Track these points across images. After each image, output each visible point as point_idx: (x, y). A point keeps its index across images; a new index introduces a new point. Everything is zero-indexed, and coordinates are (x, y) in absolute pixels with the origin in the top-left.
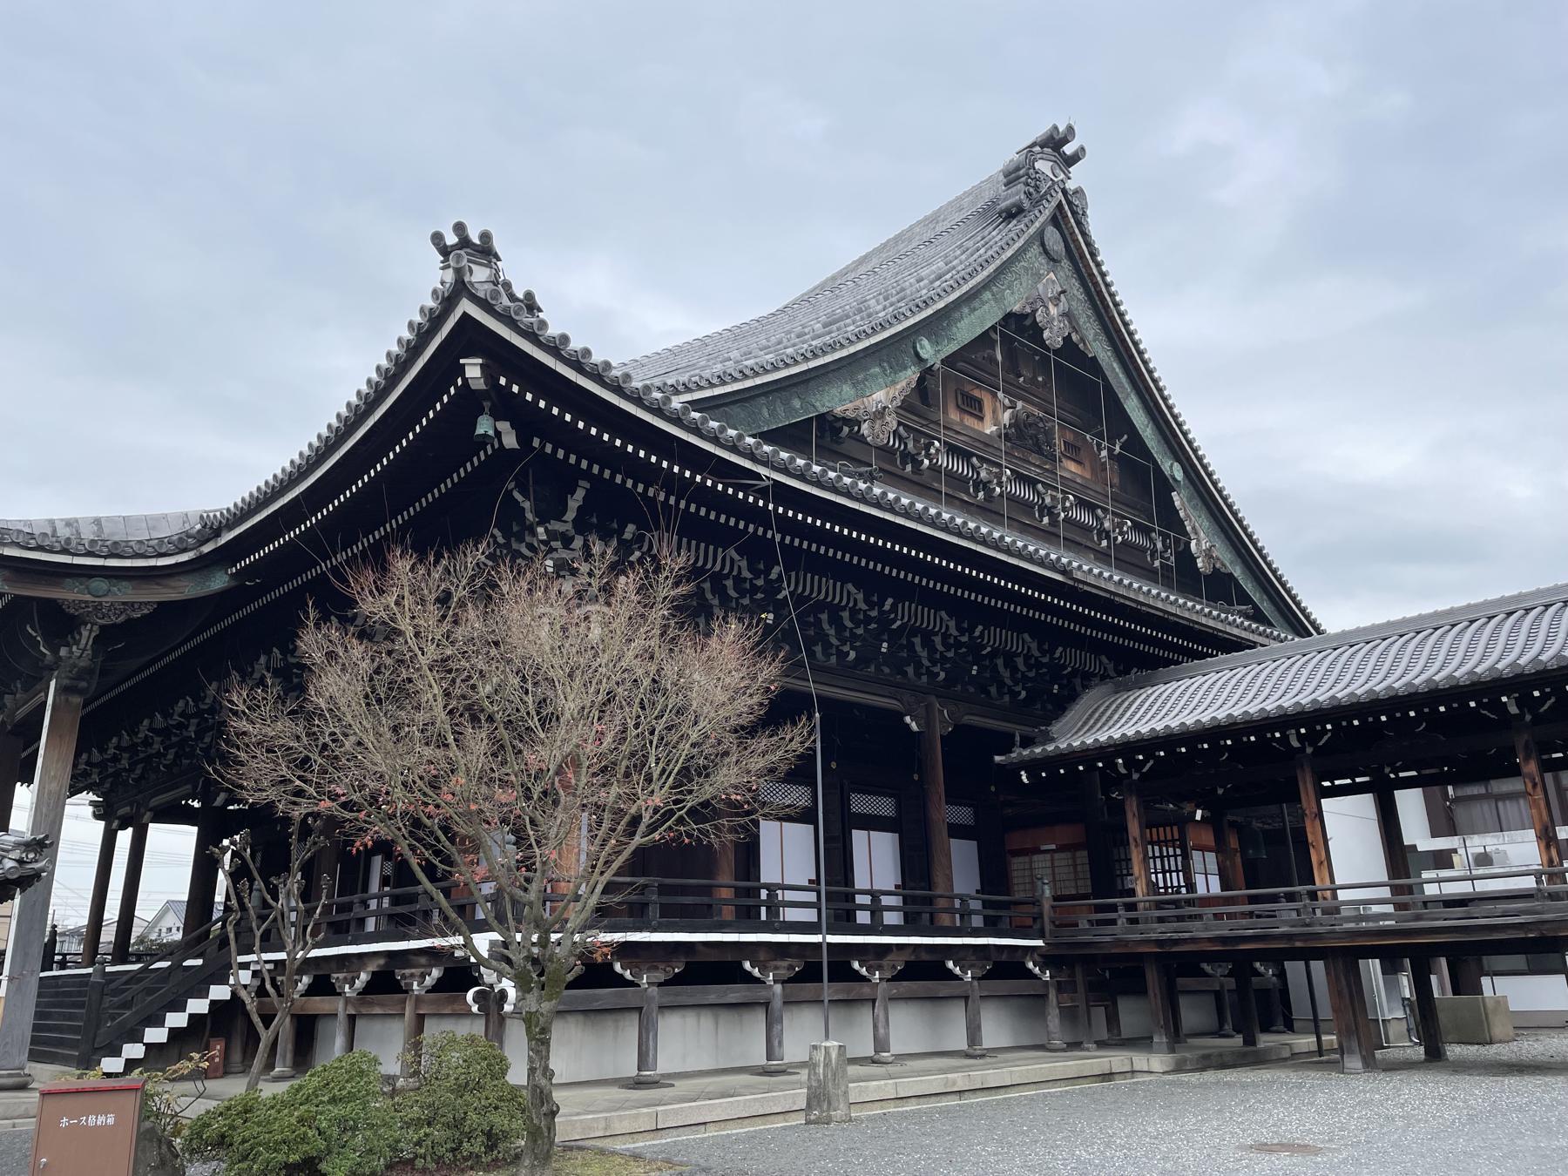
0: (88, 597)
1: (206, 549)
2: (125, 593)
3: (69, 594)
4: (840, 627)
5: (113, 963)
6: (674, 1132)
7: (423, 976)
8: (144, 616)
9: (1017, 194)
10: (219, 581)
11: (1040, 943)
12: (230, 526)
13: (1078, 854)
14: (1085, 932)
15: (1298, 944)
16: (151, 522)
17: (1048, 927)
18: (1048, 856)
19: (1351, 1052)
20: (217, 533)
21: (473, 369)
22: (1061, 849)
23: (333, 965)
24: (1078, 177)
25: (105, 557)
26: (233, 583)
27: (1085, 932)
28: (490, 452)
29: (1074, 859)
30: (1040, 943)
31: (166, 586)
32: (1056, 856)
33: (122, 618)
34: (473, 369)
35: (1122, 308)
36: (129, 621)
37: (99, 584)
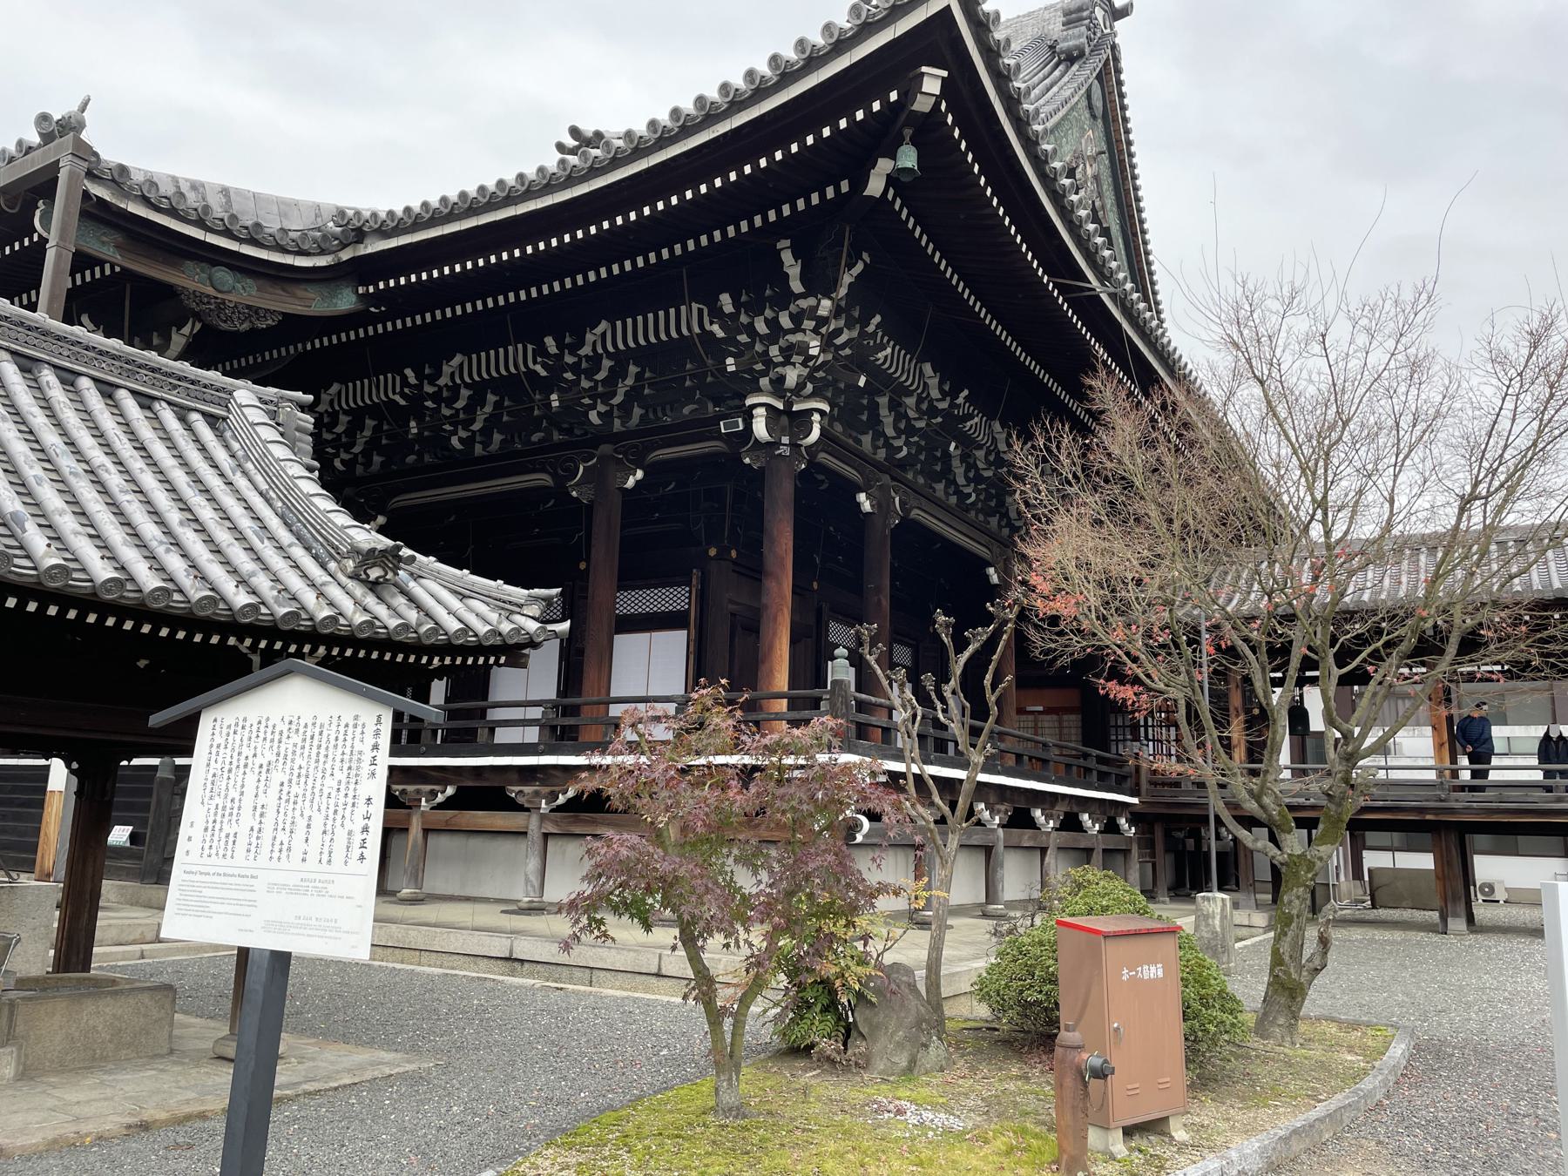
0: (210, 291)
1: (345, 255)
2: (245, 293)
3: (189, 279)
4: (970, 465)
5: (985, 770)
6: (483, 963)
7: (434, 794)
8: (269, 328)
9: (1075, 38)
10: (345, 301)
11: (1135, 800)
12: (383, 232)
13: (1065, 717)
14: (1190, 793)
15: (1428, 817)
16: (286, 207)
17: (1144, 785)
18: (1031, 717)
19: (1456, 915)
20: (359, 235)
21: (932, 82)
22: (1047, 711)
23: (515, 776)
24: (57, 117)
25: (241, 241)
26: (361, 307)
27: (1190, 793)
28: (26, 243)
29: (1060, 722)
30: (1135, 800)
31: (294, 296)
32: (1041, 717)
33: (245, 326)
34: (932, 82)
35: (1138, 182)
36: (253, 331)
37: (223, 275)
